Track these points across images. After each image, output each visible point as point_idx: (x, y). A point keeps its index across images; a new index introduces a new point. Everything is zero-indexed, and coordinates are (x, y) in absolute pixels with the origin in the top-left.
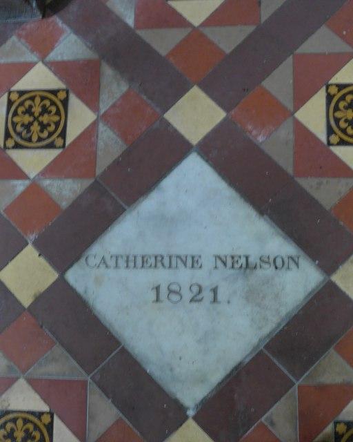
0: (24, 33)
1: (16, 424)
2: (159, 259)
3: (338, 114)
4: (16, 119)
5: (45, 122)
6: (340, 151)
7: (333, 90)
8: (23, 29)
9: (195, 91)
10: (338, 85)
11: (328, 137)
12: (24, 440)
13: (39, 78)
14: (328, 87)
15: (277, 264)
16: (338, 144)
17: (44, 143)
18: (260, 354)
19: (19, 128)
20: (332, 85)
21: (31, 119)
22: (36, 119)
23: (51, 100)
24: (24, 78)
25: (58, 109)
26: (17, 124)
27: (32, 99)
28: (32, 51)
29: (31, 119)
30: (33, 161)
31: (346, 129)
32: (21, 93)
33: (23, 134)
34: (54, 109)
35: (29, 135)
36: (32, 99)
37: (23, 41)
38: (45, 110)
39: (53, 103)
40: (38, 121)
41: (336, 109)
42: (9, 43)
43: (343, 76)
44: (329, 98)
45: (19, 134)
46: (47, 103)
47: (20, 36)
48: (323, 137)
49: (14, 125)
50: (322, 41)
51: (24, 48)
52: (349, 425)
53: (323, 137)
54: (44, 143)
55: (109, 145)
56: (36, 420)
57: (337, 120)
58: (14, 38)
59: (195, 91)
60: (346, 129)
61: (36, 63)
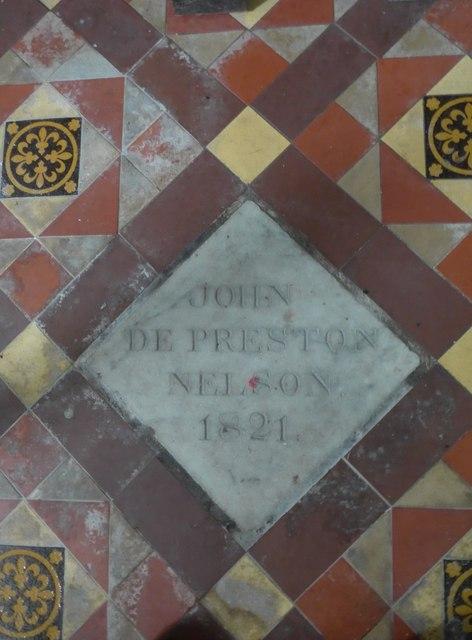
0: (435, 15)
1: (17, 566)
2: (222, 336)
3: (440, 136)
4: (67, 156)
5: (456, 131)
6: (446, 187)
7: (433, 104)
8: (434, 11)
9: (248, 112)
10: (438, 98)
11: (427, 168)
12: (463, 129)
13: (46, 104)
14: (426, 99)
15: (366, 340)
16: (441, 177)
17: (52, 189)
18: (341, 465)
19: (446, 149)
20: (431, 97)
21: (36, 158)
22: (42, 158)
23: (59, 131)
24: (445, 78)
25: (69, 143)
26: (443, 142)
27: (36, 131)
28: (452, 40)
29: (47, 157)
30: (36, 211)
31: (22, 176)
32: (443, 99)
33: (454, 158)
34: (446, 149)
35: (462, 159)
36: (36, 131)
37: (437, 27)
38: (52, 147)
39: (63, 136)
40: (38, 161)
41: (438, 128)
42: (415, 29)
43: (450, 84)
44: (428, 114)
45: (448, 157)
46: (55, 136)
47: (430, 20)
48: (420, 165)
49: (69, 149)
50: (423, 39)
51: (440, 37)
52: (467, 565)
53: (420, 165)
54: (52, 189)
55: (361, 97)
56: (12, 144)
57: (439, 144)
58: (423, 23)
59: (248, 112)
60: (22, 176)
61: (459, 58)
